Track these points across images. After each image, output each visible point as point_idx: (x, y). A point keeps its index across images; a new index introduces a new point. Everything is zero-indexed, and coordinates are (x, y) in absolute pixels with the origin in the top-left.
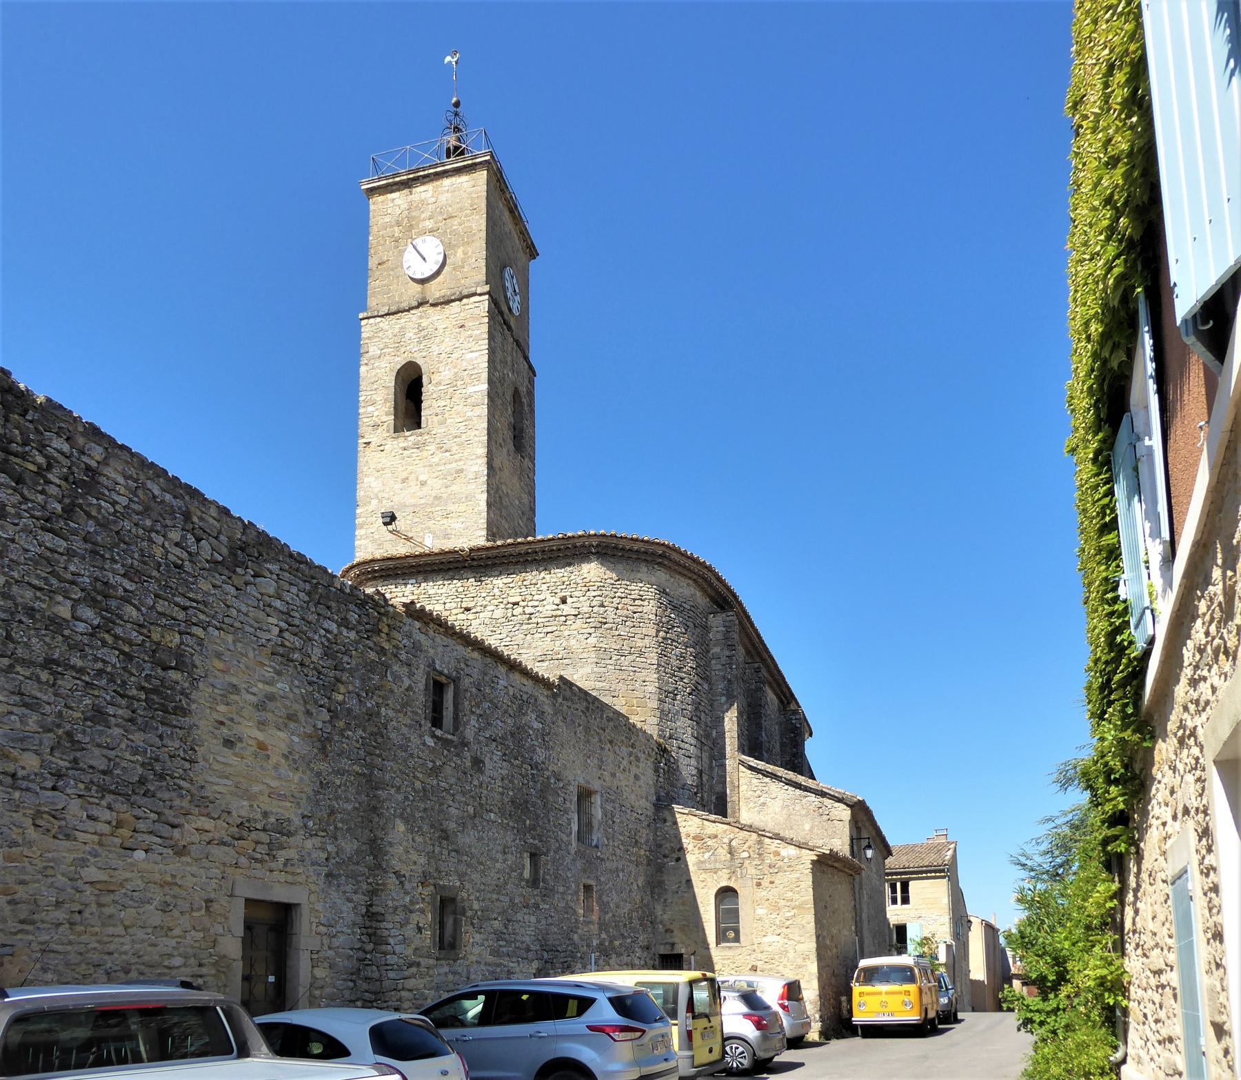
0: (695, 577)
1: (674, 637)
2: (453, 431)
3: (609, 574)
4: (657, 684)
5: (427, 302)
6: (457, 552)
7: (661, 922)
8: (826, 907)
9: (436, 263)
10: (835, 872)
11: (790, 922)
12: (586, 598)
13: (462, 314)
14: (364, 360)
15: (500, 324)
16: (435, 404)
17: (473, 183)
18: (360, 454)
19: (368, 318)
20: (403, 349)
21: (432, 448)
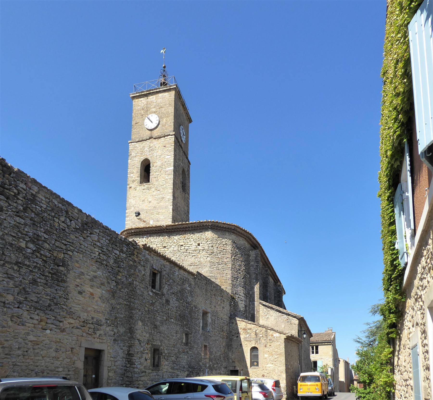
0: (245, 237)
1: (237, 258)
2: (161, 184)
3: (215, 236)
10: (293, 342)
12: (207, 244)
14: (130, 158)
16: (155, 174)
18: (128, 191)
19: (132, 143)
20: (144, 154)
21: (153, 189)
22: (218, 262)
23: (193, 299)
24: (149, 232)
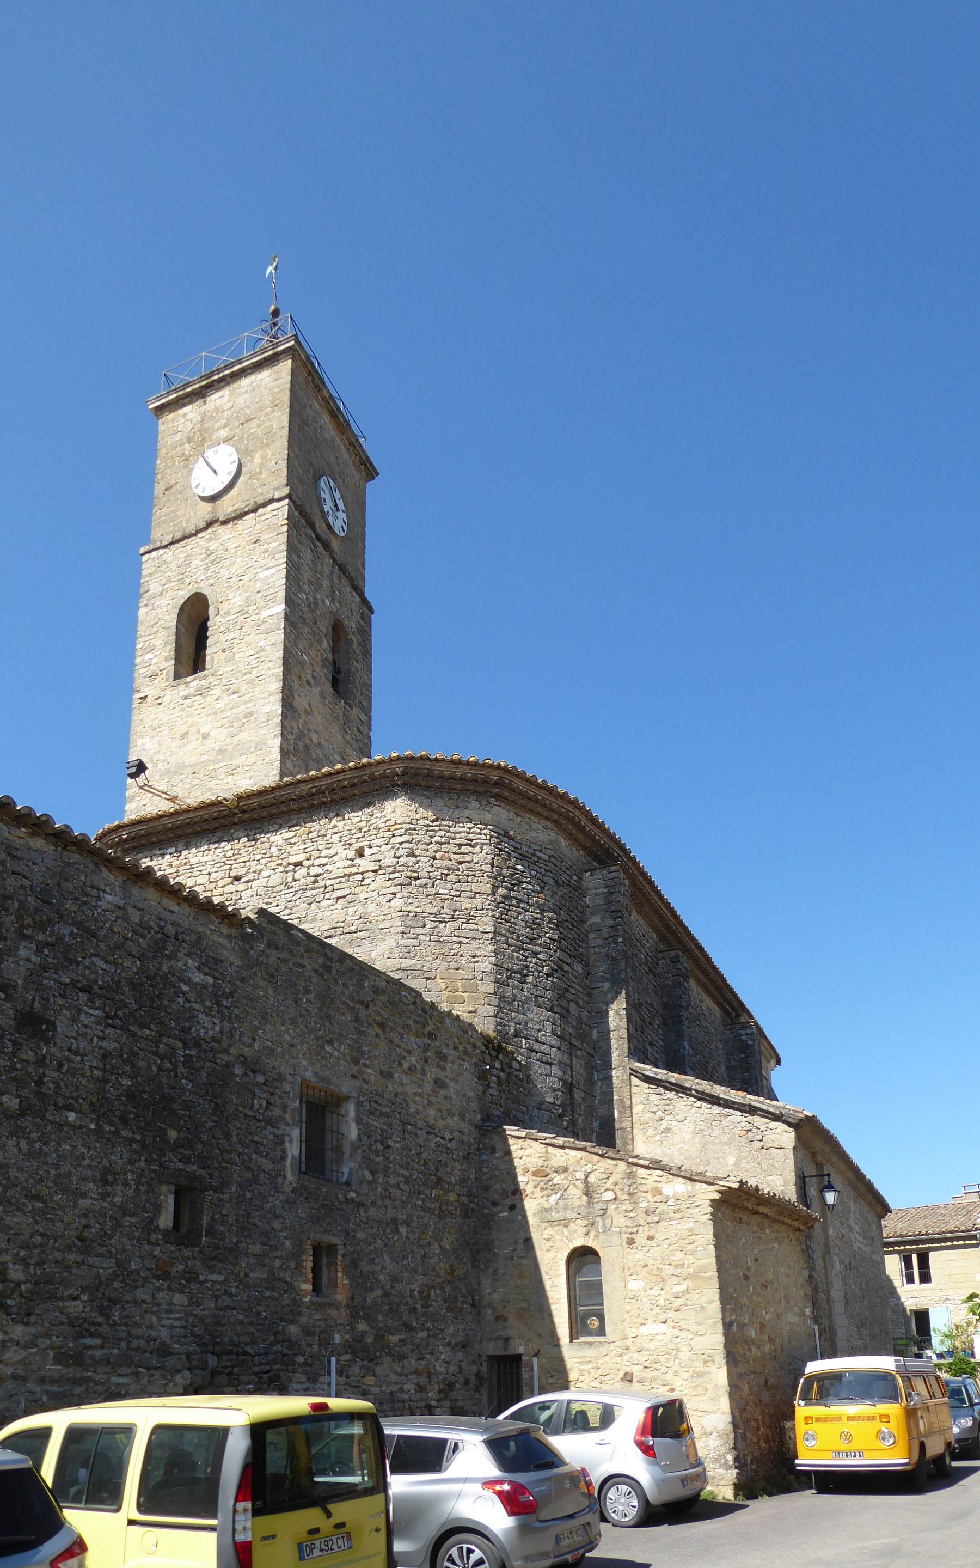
0: (555, 817)
1: (521, 895)
2: (243, 667)
3: (423, 812)
4: (493, 960)
5: (216, 521)
6: (220, 803)
7: (490, 1305)
8: (746, 1278)
9: (229, 473)
10: (766, 1223)
11: (680, 1301)
12: (390, 846)
13: (257, 527)
14: (143, 601)
15: (311, 539)
16: (223, 638)
17: (275, 376)
18: (135, 712)
19: (149, 552)
20: (188, 581)
21: (217, 691)
22: (435, 910)
23: (233, 1030)
24: (180, 832)
